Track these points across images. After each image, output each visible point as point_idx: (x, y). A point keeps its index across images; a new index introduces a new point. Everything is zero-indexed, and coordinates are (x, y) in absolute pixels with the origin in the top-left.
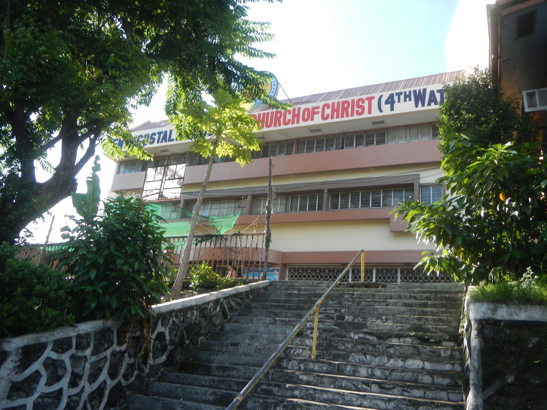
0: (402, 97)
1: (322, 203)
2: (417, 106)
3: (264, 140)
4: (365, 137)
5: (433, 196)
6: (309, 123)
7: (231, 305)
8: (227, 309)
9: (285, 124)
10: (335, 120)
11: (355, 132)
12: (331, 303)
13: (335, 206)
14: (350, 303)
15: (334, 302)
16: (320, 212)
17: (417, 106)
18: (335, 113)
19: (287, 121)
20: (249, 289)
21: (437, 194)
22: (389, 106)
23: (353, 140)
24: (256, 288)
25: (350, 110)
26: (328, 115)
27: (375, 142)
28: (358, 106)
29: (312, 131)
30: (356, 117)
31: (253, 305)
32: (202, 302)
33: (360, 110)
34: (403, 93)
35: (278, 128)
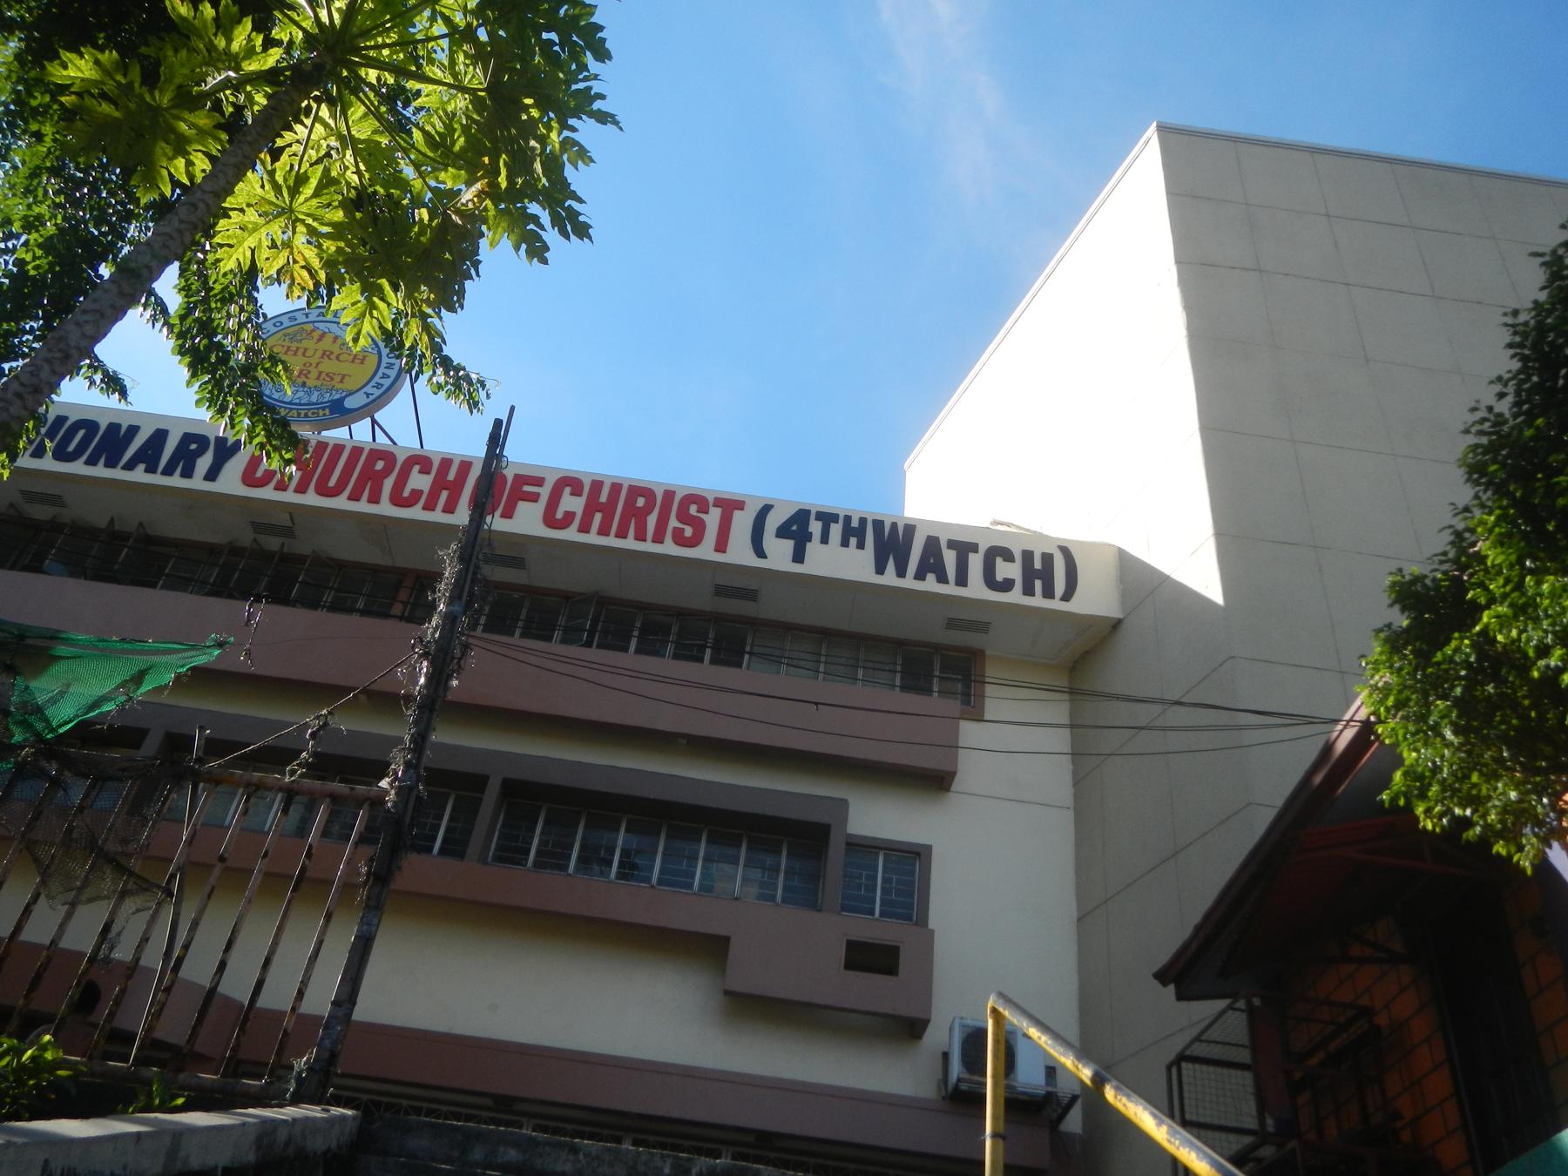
0: (836, 530)
2: (880, 570)
4: (674, 629)
5: (883, 889)
9: (397, 500)
10: (593, 538)
11: (643, 607)
13: (511, 853)
17: (880, 570)
18: (598, 517)
19: (406, 493)
20: (251, 1157)
21: (860, 889)
22: (788, 545)
25: (652, 520)
26: (569, 516)
27: (707, 657)
28: (684, 517)
30: (669, 548)
33: (688, 532)
35: (363, 506)
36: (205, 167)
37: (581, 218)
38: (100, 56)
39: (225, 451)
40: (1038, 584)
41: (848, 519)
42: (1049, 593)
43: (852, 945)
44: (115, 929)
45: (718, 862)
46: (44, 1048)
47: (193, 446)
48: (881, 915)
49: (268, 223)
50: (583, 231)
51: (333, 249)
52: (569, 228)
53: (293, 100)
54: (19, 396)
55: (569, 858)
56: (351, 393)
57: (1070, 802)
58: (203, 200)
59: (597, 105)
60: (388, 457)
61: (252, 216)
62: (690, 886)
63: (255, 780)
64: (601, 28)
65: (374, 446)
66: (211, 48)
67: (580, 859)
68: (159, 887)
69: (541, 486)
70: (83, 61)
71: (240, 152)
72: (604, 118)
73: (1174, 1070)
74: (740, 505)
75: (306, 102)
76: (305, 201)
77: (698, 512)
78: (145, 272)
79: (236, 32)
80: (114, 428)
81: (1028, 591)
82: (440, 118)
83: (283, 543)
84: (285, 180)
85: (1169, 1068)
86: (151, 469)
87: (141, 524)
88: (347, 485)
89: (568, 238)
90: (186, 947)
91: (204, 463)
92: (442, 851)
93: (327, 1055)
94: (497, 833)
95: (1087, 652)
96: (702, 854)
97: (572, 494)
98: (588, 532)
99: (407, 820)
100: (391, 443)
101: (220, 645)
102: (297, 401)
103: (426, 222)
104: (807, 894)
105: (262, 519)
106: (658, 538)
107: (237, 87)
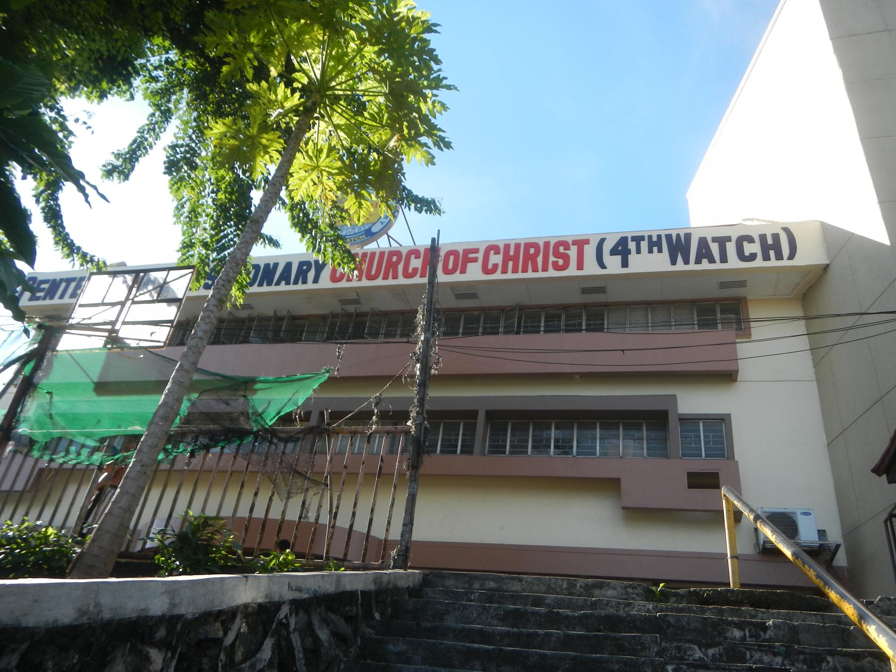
0: (644, 245)
1: (473, 440)
2: (674, 262)
3: (357, 306)
4: (563, 317)
6: (457, 277)
7: (316, 639)
8: (299, 655)
9: (407, 275)
10: (510, 276)
12: (698, 654)
13: (497, 448)
14: (779, 660)
15: (711, 652)
16: (466, 457)
17: (674, 262)
18: (511, 264)
20: (372, 587)
21: (691, 444)
22: (618, 258)
23: (540, 322)
24: (391, 586)
25: (540, 260)
26: (495, 266)
28: (557, 254)
29: (459, 296)
30: (552, 273)
31: (391, 647)
32: (203, 605)
33: (561, 262)
34: (646, 238)
35: (390, 282)
36: (278, 157)
37: (446, 140)
38: (224, 121)
39: (320, 267)
40: (772, 253)
41: (650, 237)
42: (779, 257)
43: (690, 475)
44: (307, 503)
45: (608, 439)
46: (287, 555)
47: (305, 268)
48: (706, 456)
49: (310, 174)
50: (448, 145)
51: (341, 180)
52: (442, 145)
53: (306, 122)
54: (223, 285)
55: (527, 447)
56: (374, 224)
57: (813, 377)
58: (277, 181)
59: (444, 82)
60: (398, 253)
61: (302, 173)
62: (595, 454)
63: (353, 430)
64: (435, 50)
65: (391, 249)
66: (270, 101)
67: (533, 447)
68: (322, 483)
69: (478, 253)
70: (218, 125)
71: (288, 154)
72: (449, 87)
73: (888, 523)
74: (587, 242)
75: (312, 121)
76: (323, 160)
77: (564, 250)
78: (261, 220)
79: (278, 91)
80: (267, 266)
81: (766, 258)
82: (375, 105)
83: (356, 308)
84: (313, 153)
85: (886, 522)
86: (288, 283)
87: (289, 311)
88: (380, 273)
89: (443, 150)
90: (338, 507)
91: (311, 275)
92: (462, 452)
93: (404, 548)
94: (488, 439)
95: (811, 287)
96: (598, 436)
97: (495, 254)
98: (507, 273)
99: (422, 439)
100: (399, 246)
101: (328, 372)
102: (349, 234)
103: (377, 158)
104: (660, 449)
105: (344, 297)
106: (545, 269)
107: (285, 115)
